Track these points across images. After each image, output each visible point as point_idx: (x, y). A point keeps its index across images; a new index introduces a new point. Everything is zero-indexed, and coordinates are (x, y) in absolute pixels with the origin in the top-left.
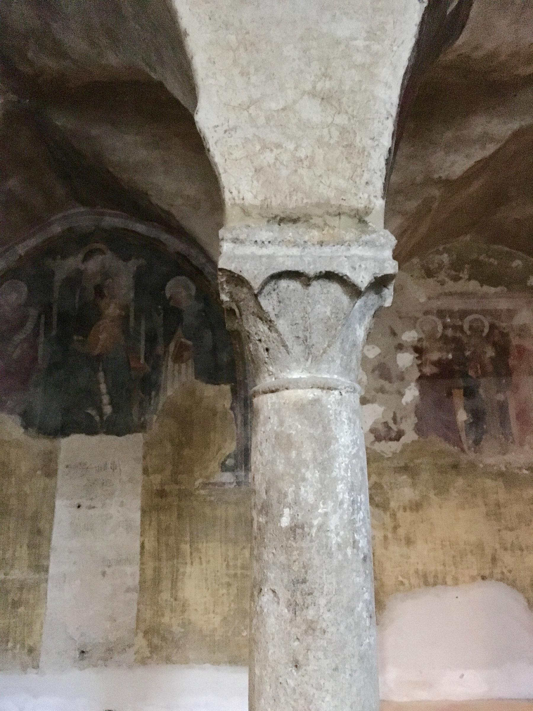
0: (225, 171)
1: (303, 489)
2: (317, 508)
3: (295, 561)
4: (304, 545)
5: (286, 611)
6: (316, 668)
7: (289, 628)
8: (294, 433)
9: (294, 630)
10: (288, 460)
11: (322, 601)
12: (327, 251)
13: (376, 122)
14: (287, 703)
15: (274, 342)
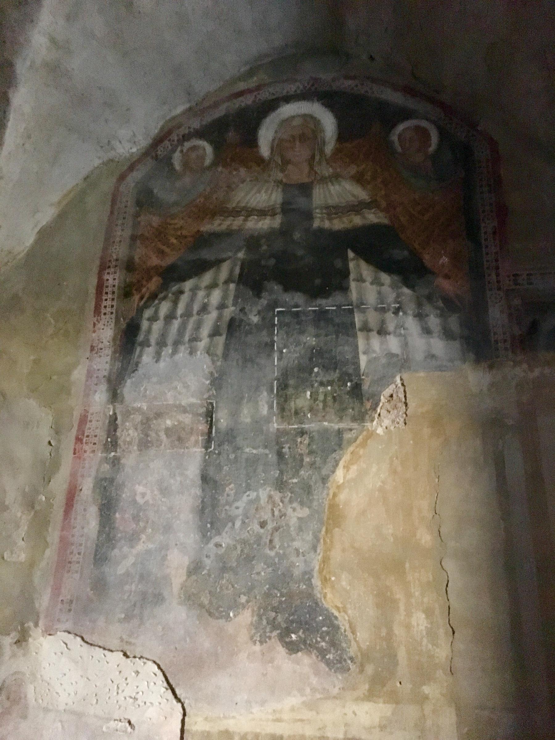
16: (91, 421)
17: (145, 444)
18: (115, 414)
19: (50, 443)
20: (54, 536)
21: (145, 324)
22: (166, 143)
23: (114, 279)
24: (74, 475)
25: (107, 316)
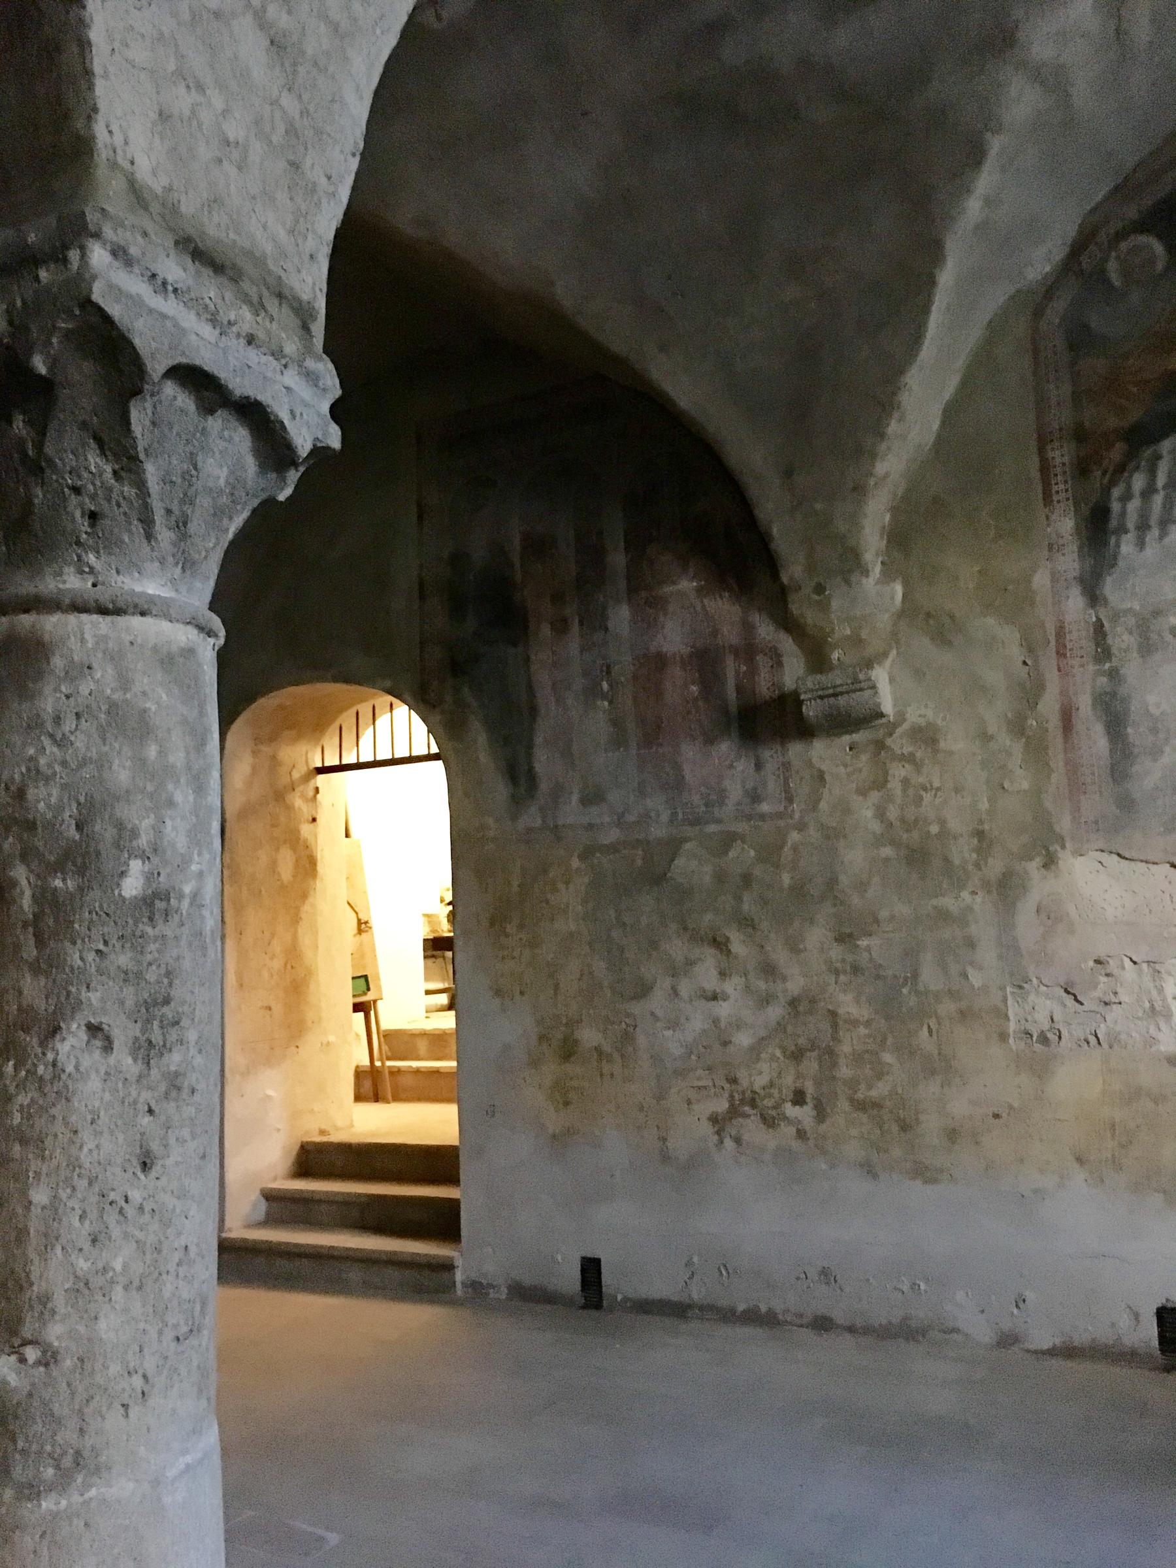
0: (106, 76)
1: (169, 823)
2: (191, 860)
3: (150, 964)
4: (169, 933)
5: (130, 1060)
6: (179, 1159)
7: (134, 1093)
8: (153, 708)
9: (146, 1095)
10: (141, 762)
11: (192, 1036)
12: (253, 356)
13: (338, 148)
14: (126, 1236)
15: (119, 505)
16: (1070, 632)
17: (1147, 648)
18: (1099, 620)
19: (1025, 663)
20: (1058, 761)
21: (1115, 507)
22: (1092, 247)
23: (1061, 455)
24: (1064, 693)
25: (1062, 504)
